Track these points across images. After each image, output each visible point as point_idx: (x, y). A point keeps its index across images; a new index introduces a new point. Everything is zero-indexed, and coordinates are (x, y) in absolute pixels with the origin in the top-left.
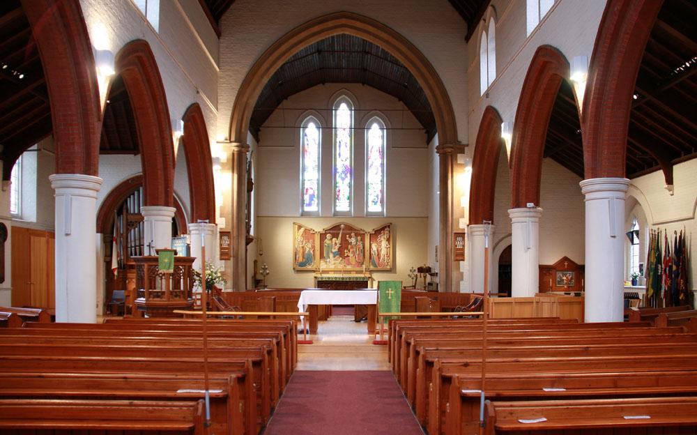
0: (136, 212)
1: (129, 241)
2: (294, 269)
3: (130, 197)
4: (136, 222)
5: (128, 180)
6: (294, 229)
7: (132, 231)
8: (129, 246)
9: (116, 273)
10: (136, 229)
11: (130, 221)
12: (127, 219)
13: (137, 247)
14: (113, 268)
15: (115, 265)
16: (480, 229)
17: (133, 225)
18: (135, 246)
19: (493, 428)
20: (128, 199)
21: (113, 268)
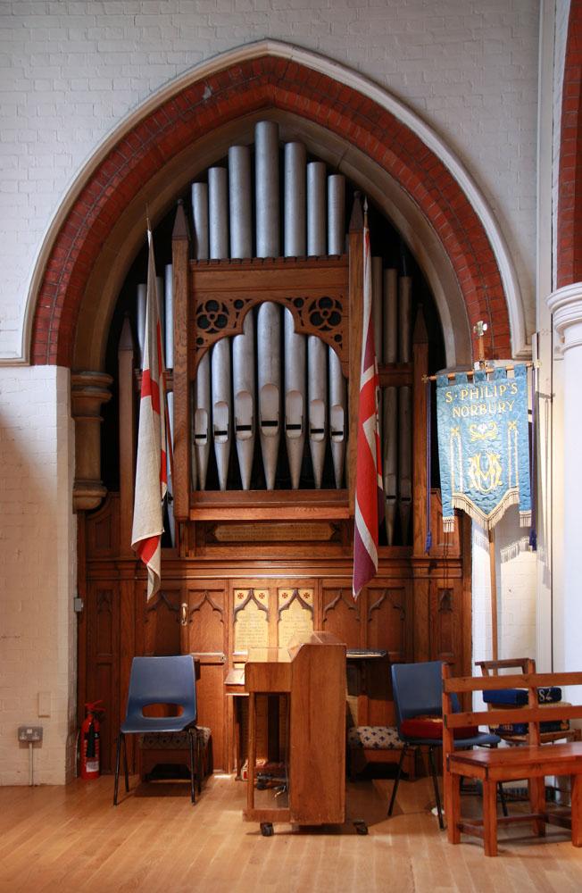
0: (263, 250)
1: (201, 403)
3: (204, 179)
4: (238, 304)
5: (199, 85)
7: (218, 353)
8: (203, 429)
9: (153, 564)
10: (238, 340)
11: (202, 299)
12: (191, 293)
13: (267, 430)
14: (136, 538)
15: (145, 522)
16: (130, 567)
17: (221, 322)
18: (257, 424)
19: (293, 796)
20: (196, 188)
21: (136, 538)
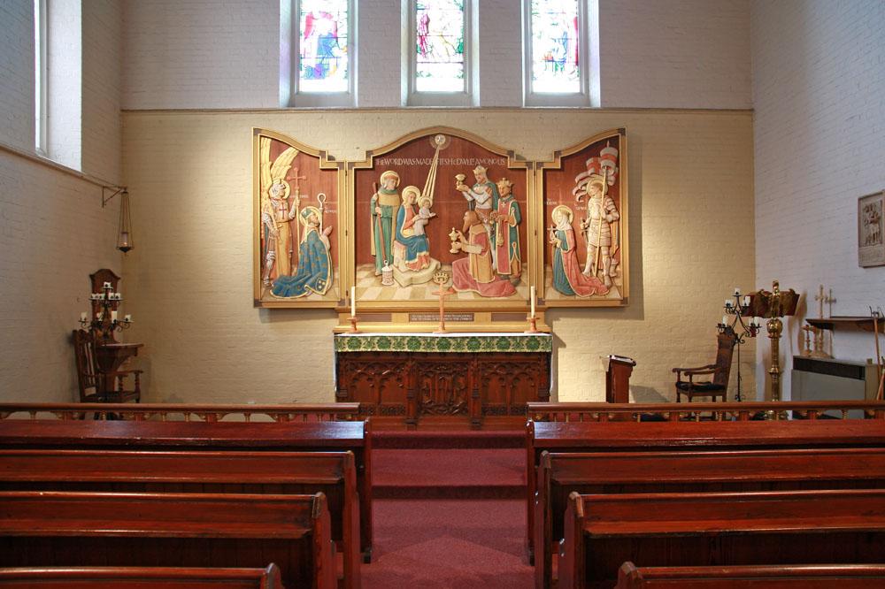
2: (257, 303)
6: (257, 150)
